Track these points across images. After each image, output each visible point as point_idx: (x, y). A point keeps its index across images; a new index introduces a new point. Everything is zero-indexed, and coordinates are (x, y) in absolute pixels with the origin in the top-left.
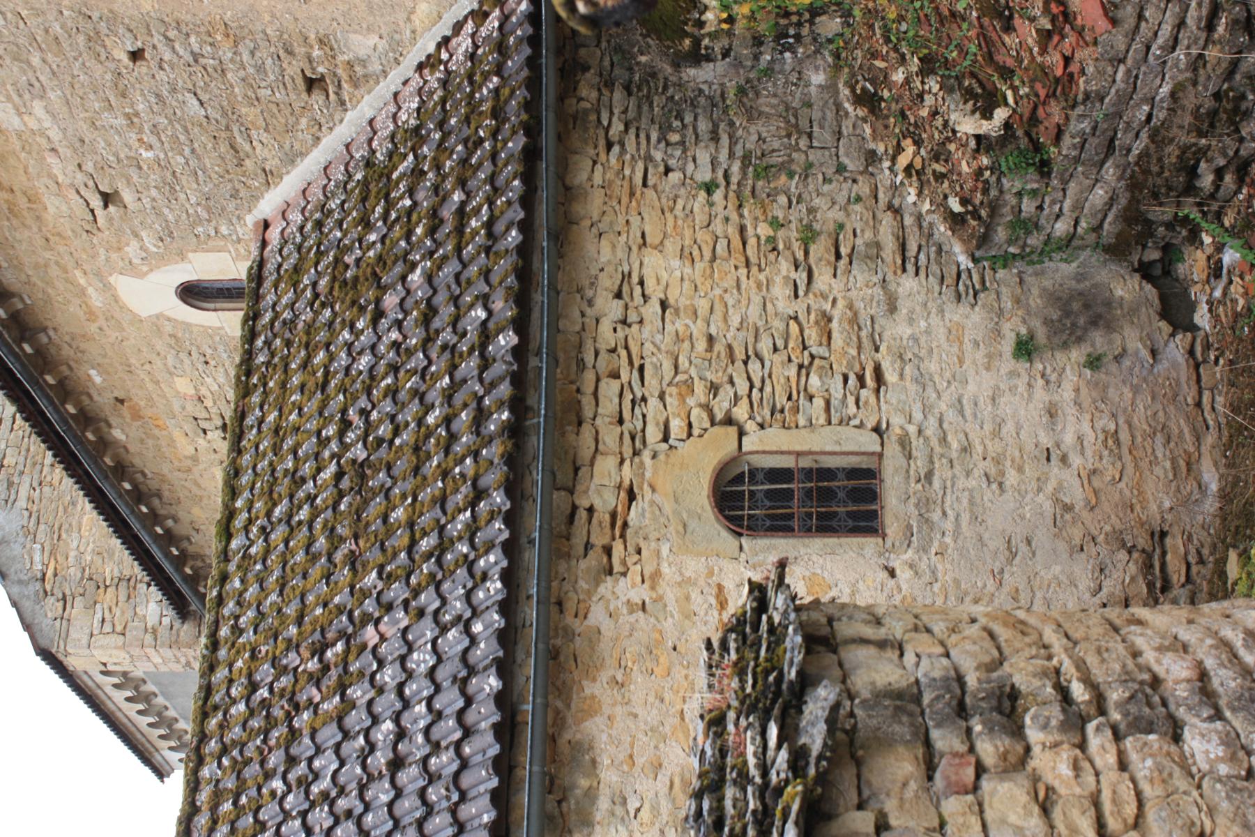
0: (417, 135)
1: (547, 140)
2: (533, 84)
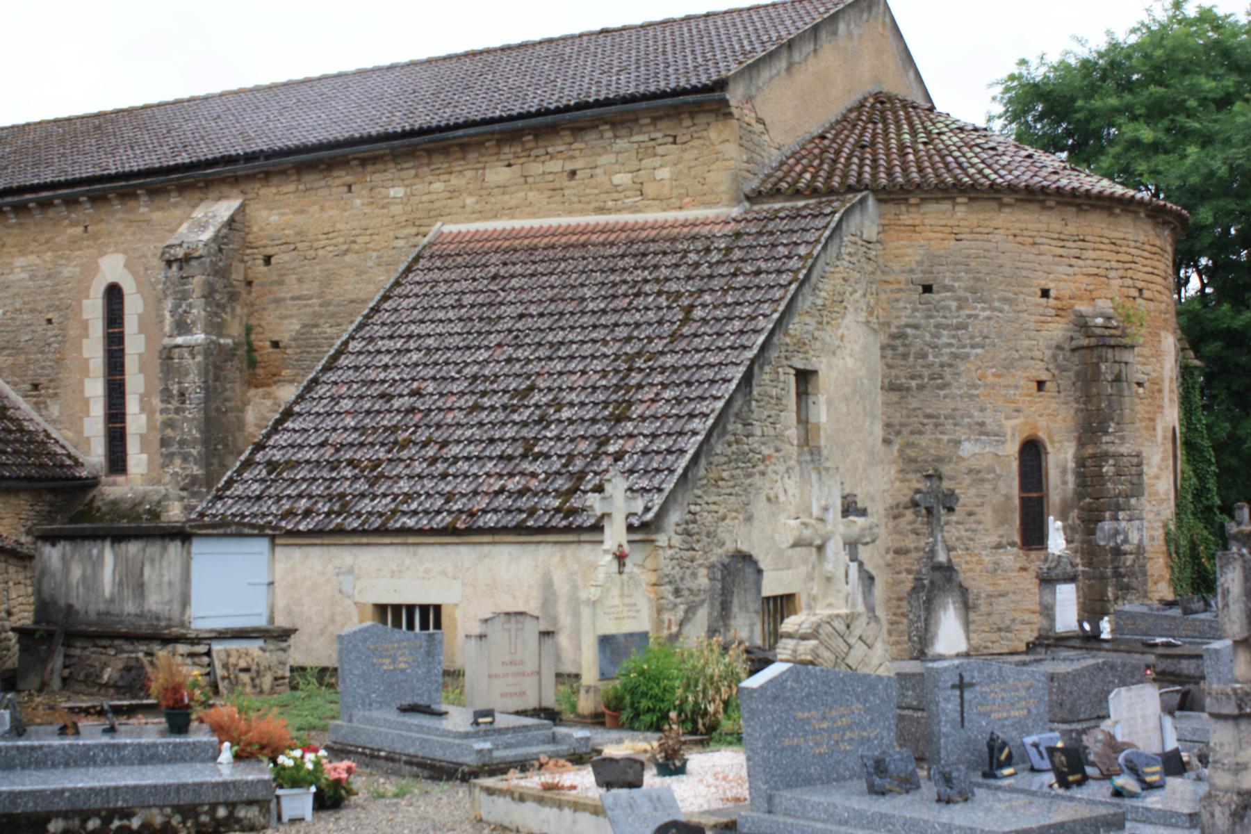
0: (21, 430)
1: (36, 485)
2: (54, 479)
